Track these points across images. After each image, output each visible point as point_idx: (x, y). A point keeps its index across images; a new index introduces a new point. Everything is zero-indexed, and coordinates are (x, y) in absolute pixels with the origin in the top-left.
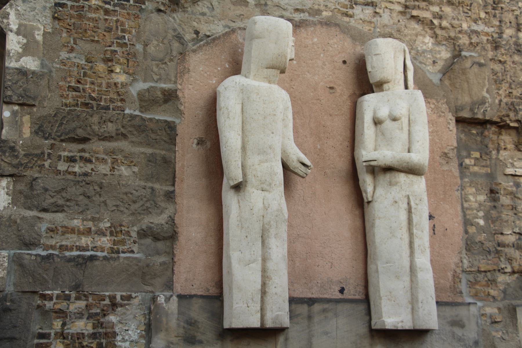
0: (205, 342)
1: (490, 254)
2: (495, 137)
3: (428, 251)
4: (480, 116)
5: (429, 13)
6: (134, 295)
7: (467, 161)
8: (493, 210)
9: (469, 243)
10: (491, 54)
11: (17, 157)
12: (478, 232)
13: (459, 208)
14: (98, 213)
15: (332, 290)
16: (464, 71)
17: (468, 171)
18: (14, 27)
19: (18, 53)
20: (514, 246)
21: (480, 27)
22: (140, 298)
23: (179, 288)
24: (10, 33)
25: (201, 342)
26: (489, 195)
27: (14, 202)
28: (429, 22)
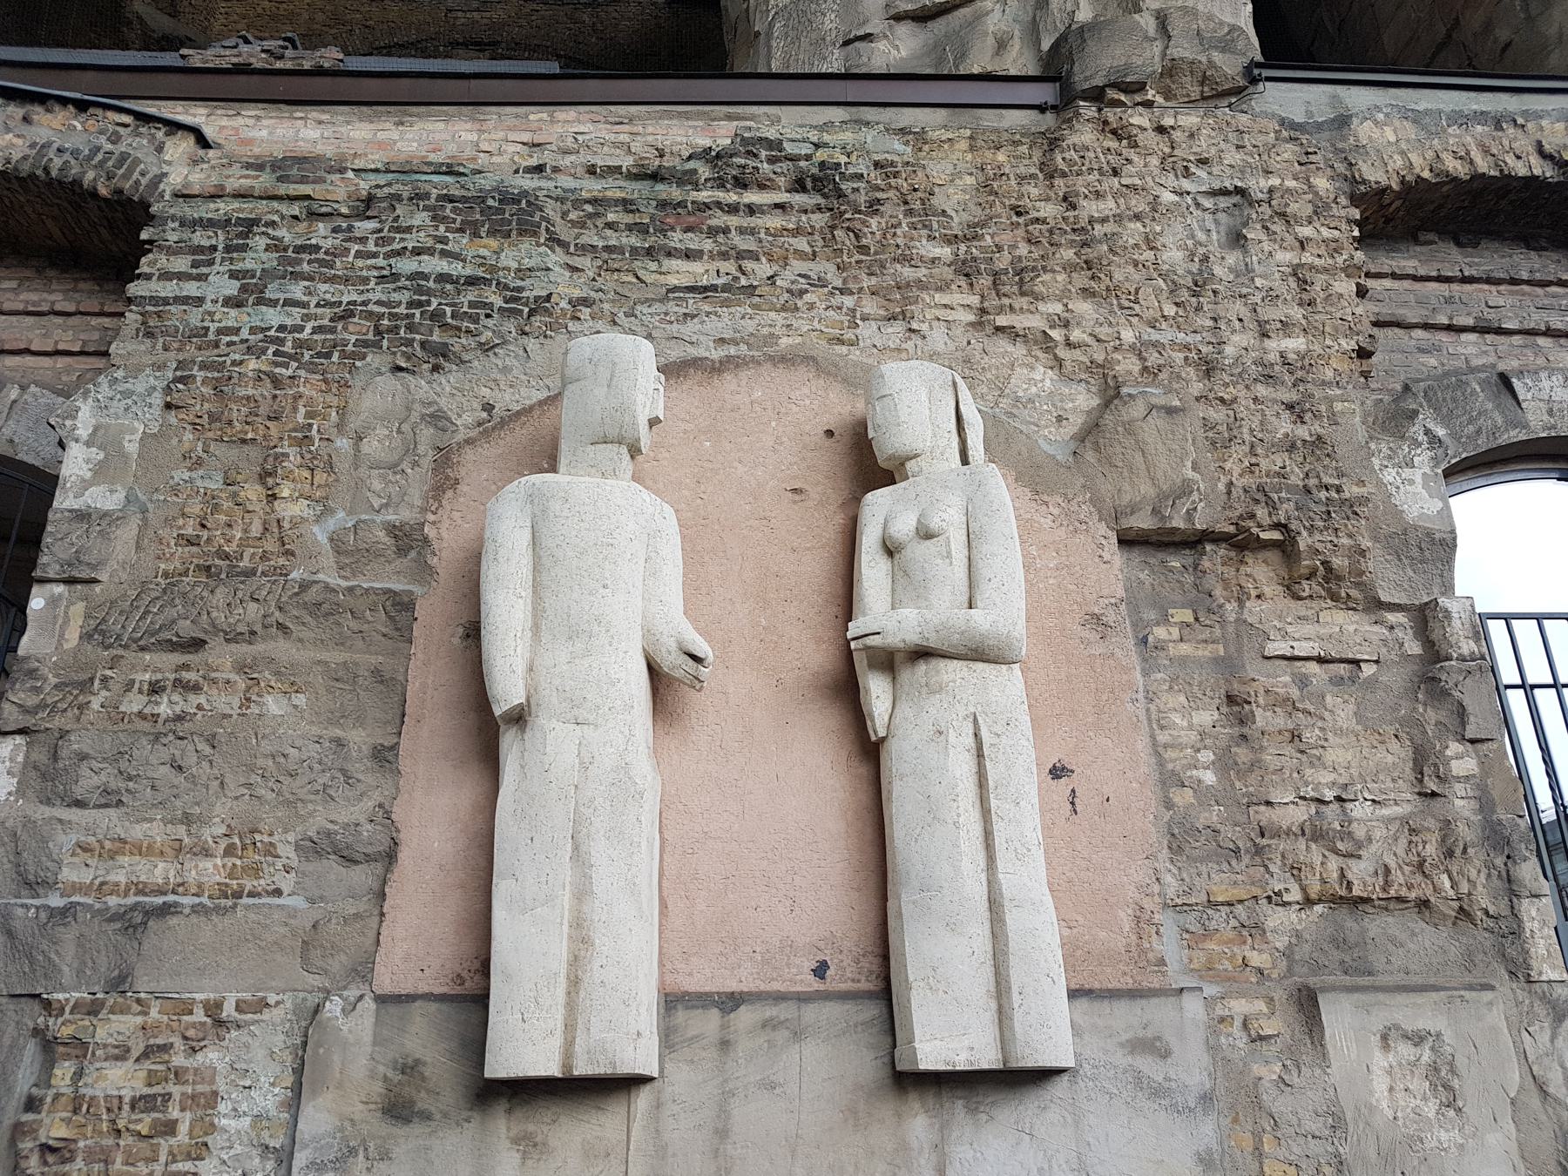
0: (438, 1116)
1: (1239, 858)
2: (1230, 572)
3: (1039, 855)
4: (1178, 523)
5: (1038, 316)
6: (272, 998)
7: (1160, 632)
8: (1238, 745)
9: (1176, 831)
10: (1197, 388)
11: (37, 690)
13: (1142, 744)
14: (198, 804)
15: (794, 970)
16: (1129, 428)
18: (83, 432)
19: (84, 480)
20: (1303, 834)
21: (1166, 335)
22: (289, 1005)
23: (387, 979)
24: (73, 444)
25: (426, 1116)
26: (1224, 709)
27: (20, 791)
28: (1039, 336)
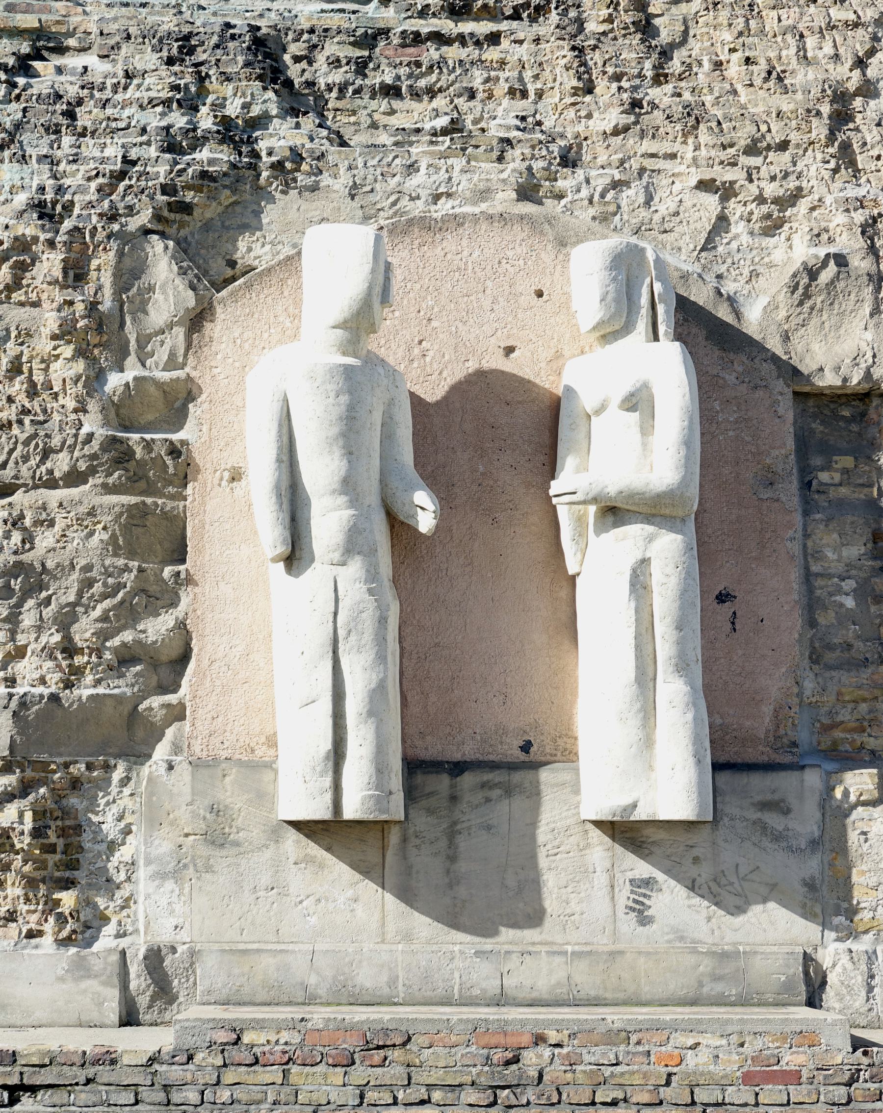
12: (840, 623)
17: (823, 497)
